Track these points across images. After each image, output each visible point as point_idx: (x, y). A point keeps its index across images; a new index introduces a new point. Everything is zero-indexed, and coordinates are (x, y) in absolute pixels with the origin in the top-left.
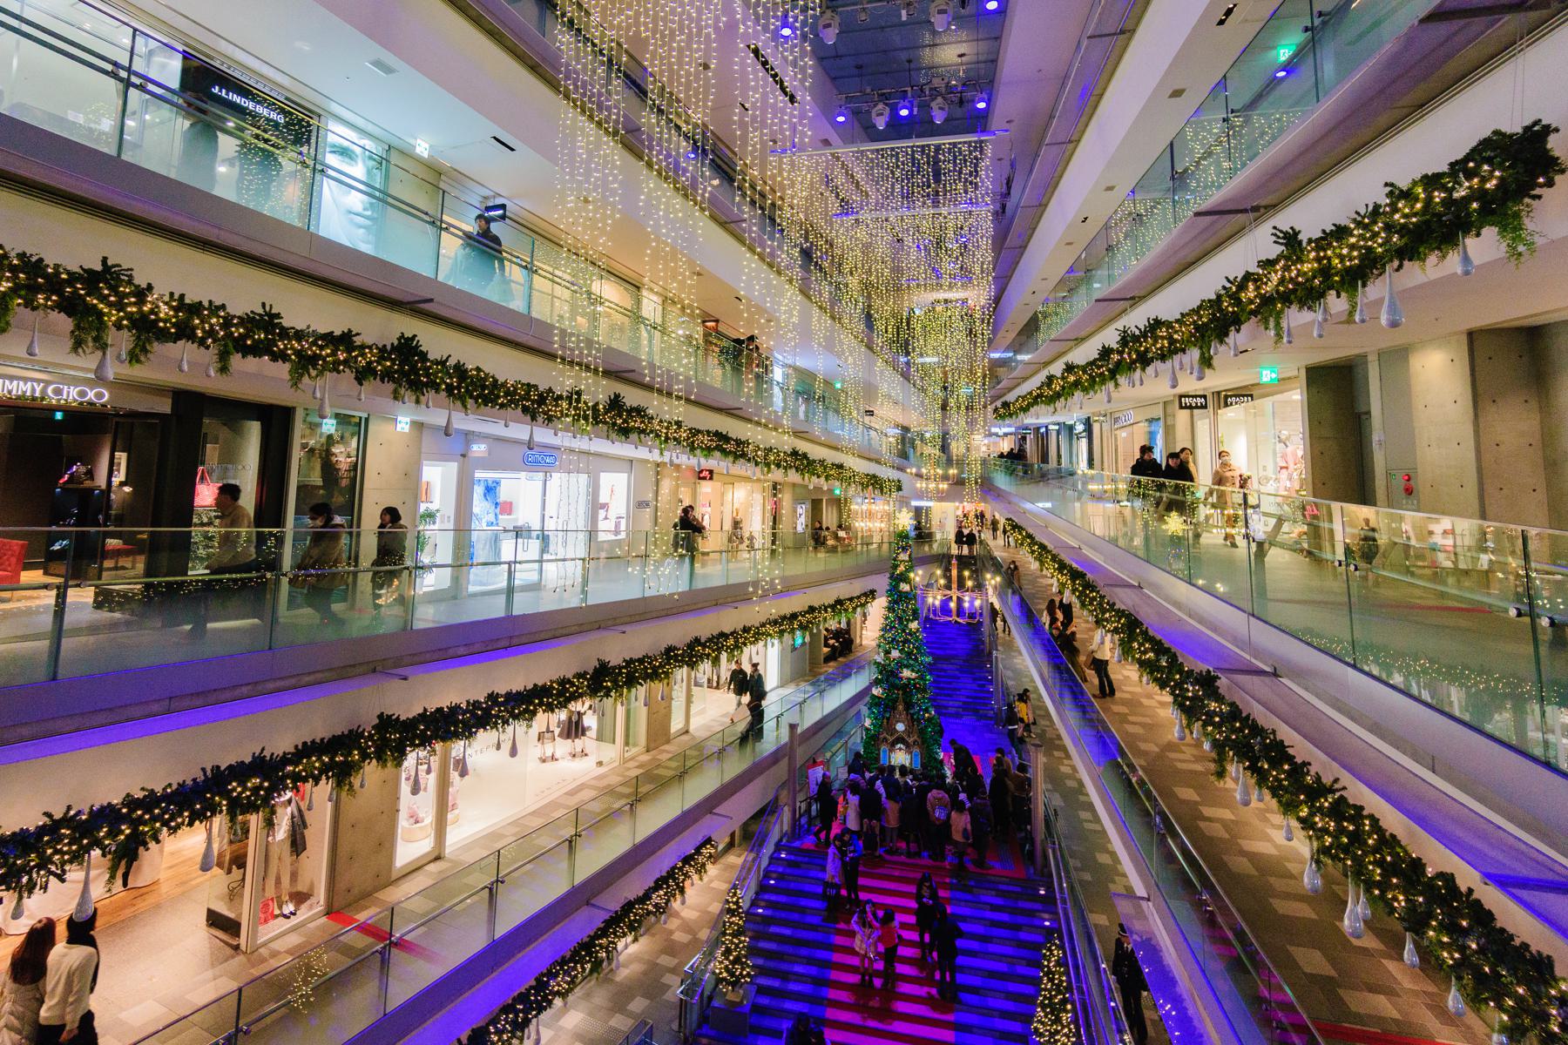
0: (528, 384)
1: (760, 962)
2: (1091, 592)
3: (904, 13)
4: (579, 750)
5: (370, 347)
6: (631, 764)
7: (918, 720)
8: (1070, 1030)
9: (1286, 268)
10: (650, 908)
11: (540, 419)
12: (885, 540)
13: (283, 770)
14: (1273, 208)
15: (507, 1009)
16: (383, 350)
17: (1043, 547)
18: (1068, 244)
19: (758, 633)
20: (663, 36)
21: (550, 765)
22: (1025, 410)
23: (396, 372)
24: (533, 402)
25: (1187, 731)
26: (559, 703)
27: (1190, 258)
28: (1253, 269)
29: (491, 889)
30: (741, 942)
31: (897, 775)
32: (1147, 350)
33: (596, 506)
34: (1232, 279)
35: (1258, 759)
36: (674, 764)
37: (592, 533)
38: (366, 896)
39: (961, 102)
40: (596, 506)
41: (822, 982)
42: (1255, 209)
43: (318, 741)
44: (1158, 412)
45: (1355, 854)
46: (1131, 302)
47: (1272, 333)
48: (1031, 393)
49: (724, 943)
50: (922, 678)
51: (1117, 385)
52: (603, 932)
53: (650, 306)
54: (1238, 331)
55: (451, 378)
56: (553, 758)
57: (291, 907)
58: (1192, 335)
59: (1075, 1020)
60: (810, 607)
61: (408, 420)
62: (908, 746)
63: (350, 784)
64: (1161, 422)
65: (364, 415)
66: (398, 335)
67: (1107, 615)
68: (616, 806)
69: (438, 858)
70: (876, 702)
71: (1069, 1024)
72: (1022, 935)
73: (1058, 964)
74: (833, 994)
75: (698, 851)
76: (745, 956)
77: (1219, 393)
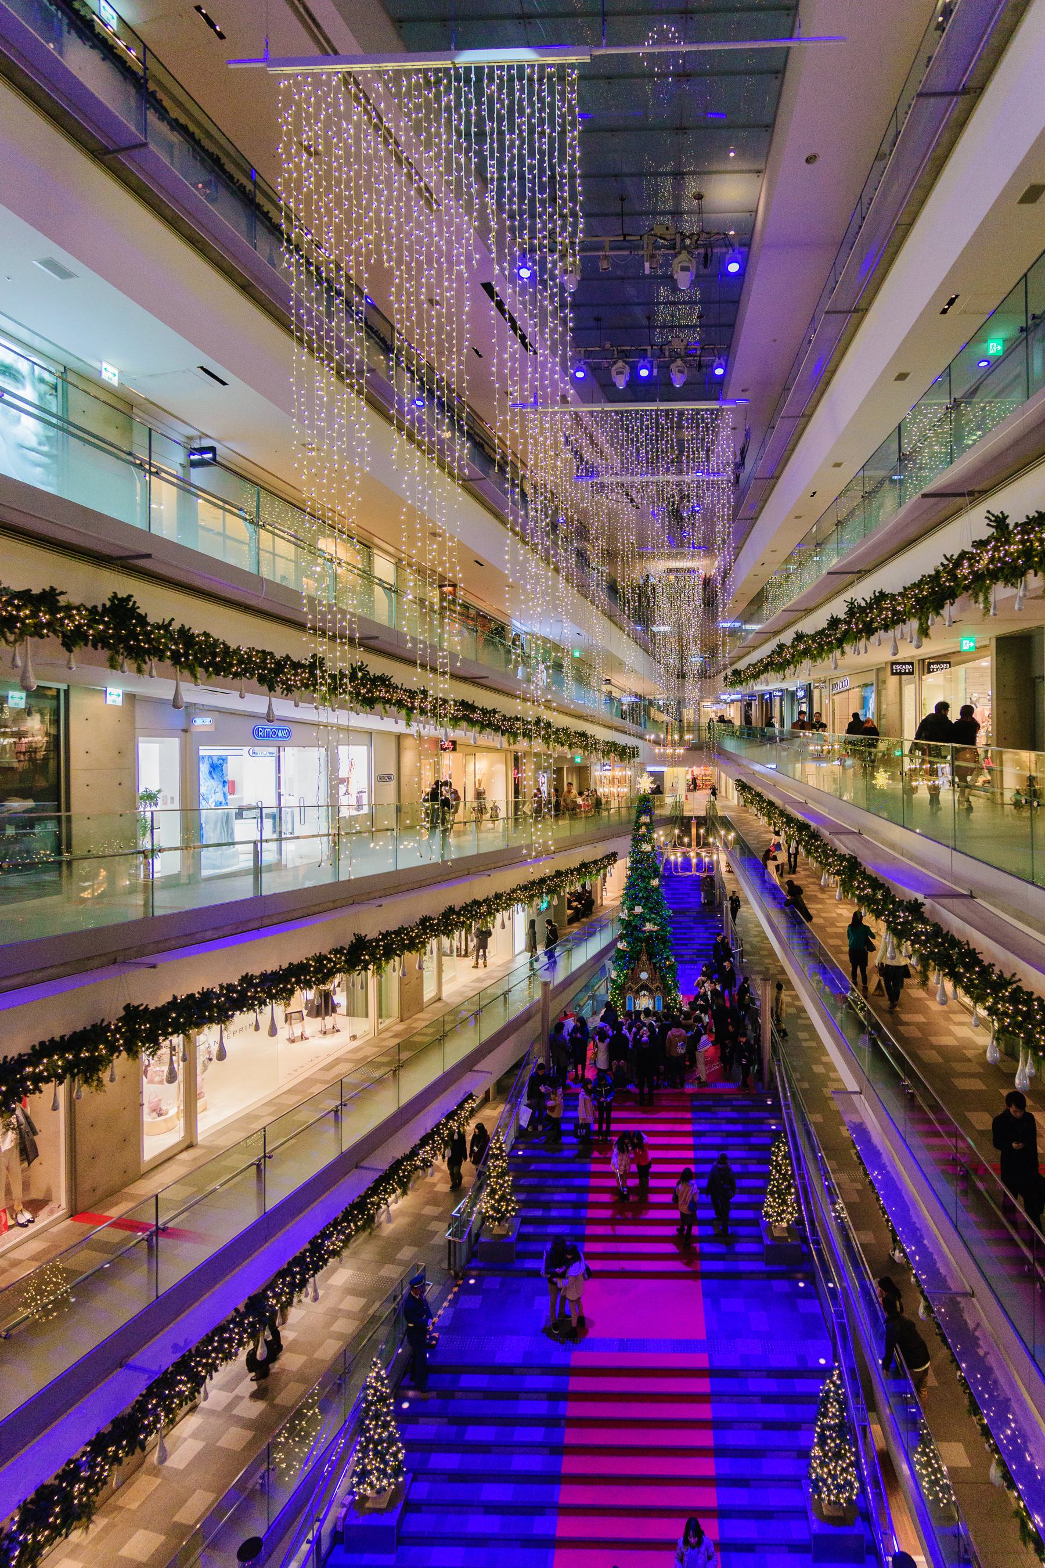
0: (263, 652)
1: (523, 1197)
2: (816, 841)
3: (647, 265)
4: (329, 1026)
5: (78, 608)
6: (385, 1035)
7: (660, 968)
8: (794, 1209)
9: (996, 549)
10: (418, 1163)
11: (278, 690)
12: (623, 805)
13: (20, 1073)
14: (984, 493)
15: (282, 1274)
16: (93, 611)
17: (771, 804)
18: (797, 517)
19: (510, 899)
20: (409, 270)
21: (299, 1045)
22: (756, 676)
23: (111, 636)
24: (270, 670)
25: (897, 951)
26: (317, 979)
27: (912, 536)
28: (969, 548)
29: (258, 1166)
30: (505, 1182)
31: (642, 1017)
32: (872, 621)
33: (335, 782)
34: (948, 556)
35: (955, 966)
36: (431, 1030)
37: (334, 806)
38: (113, 1193)
39: (700, 366)
40: (335, 782)
41: (582, 1205)
42: (971, 493)
43: (57, 1039)
44: (871, 678)
45: (1027, 1028)
46: (858, 575)
47: (982, 606)
48: (762, 661)
49: (489, 1185)
50: (663, 929)
51: (843, 653)
52: (374, 1190)
53: (384, 568)
54: (952, 604)
55: (176, 644)
56: (303, 1037)
57: (28, 1216)
58: (913, 607)
59: (797, 1200)
60: (557, 872)
61: (120, 692)
62: (651, 991)
63: (100, 1081)
64: (874, 688)
65: (63, 687)
66: (110, 595)
67: (831, 860)
68: (377, 1074)
69: (191, 1146)
70: (621, 955)
71: (792, 1204)
72: (753, 1140)
73: (785, 1157)
74: (591, 1213)
75: (461, 1106)
76: (510, 1194)
77: (923, 660)
